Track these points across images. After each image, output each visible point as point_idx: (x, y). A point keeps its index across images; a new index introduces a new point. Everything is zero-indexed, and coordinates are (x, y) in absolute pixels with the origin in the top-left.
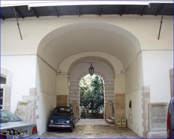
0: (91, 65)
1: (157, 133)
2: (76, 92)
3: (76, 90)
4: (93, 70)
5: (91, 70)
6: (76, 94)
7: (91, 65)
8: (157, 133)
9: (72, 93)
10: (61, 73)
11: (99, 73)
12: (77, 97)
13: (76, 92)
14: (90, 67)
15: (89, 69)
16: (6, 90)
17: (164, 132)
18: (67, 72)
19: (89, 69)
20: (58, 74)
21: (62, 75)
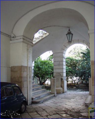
0: (69, 30)
1: (82, 85)
2: (59, 63)
3: (60, 61)
4: (71, 35)
5: (68, 35)
6: (60, 66)
7: (69, 30)
8: (82, 85)
9: (57, 64)
10: (16, 37)
11: (84, 41)
12: (62, 69)
13: (59, 63)
14: (68, 32)
15: (66, 35)
16: (27, 70)
17: (4, 79)
18: (22, 35)
19: (66, 35)
20: (12, 39)
21: (16, 39)
